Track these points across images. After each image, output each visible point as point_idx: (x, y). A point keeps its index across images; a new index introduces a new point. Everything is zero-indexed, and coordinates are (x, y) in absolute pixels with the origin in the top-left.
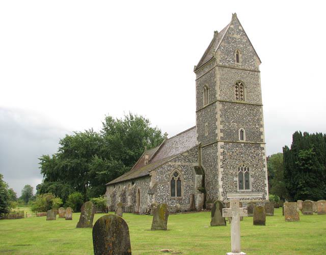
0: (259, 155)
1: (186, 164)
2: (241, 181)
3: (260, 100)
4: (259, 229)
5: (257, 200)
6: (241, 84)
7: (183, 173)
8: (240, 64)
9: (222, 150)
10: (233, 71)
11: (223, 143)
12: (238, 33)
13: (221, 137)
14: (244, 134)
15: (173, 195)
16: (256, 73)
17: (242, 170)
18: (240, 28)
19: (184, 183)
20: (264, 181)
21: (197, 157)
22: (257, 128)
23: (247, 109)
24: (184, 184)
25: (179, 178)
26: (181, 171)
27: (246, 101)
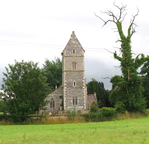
0: (82, 91)
1: (56, 95)
2: (73, 102)
3: (83, 68)
4: (115, 127)
5: (80, 109)
6: (75, 63)
7: (55, 98)
8: (75, 54)
9: (65, 90)
10: (71, 58)
11: (66, 88)
12: (74, 40)
13: (65, 85)
14: (76, 83)
15: (51, 107)
16: (82, 57)
17: (74, 97)
18: (75, 38)
19: (56, 102)
20: (84, 102)
21: (61, 92)
22: (81, 81)
23: (77, 73)
24: (56, 102)
25: (54, 101)
26: (54, 98)
27: (77, 70)
